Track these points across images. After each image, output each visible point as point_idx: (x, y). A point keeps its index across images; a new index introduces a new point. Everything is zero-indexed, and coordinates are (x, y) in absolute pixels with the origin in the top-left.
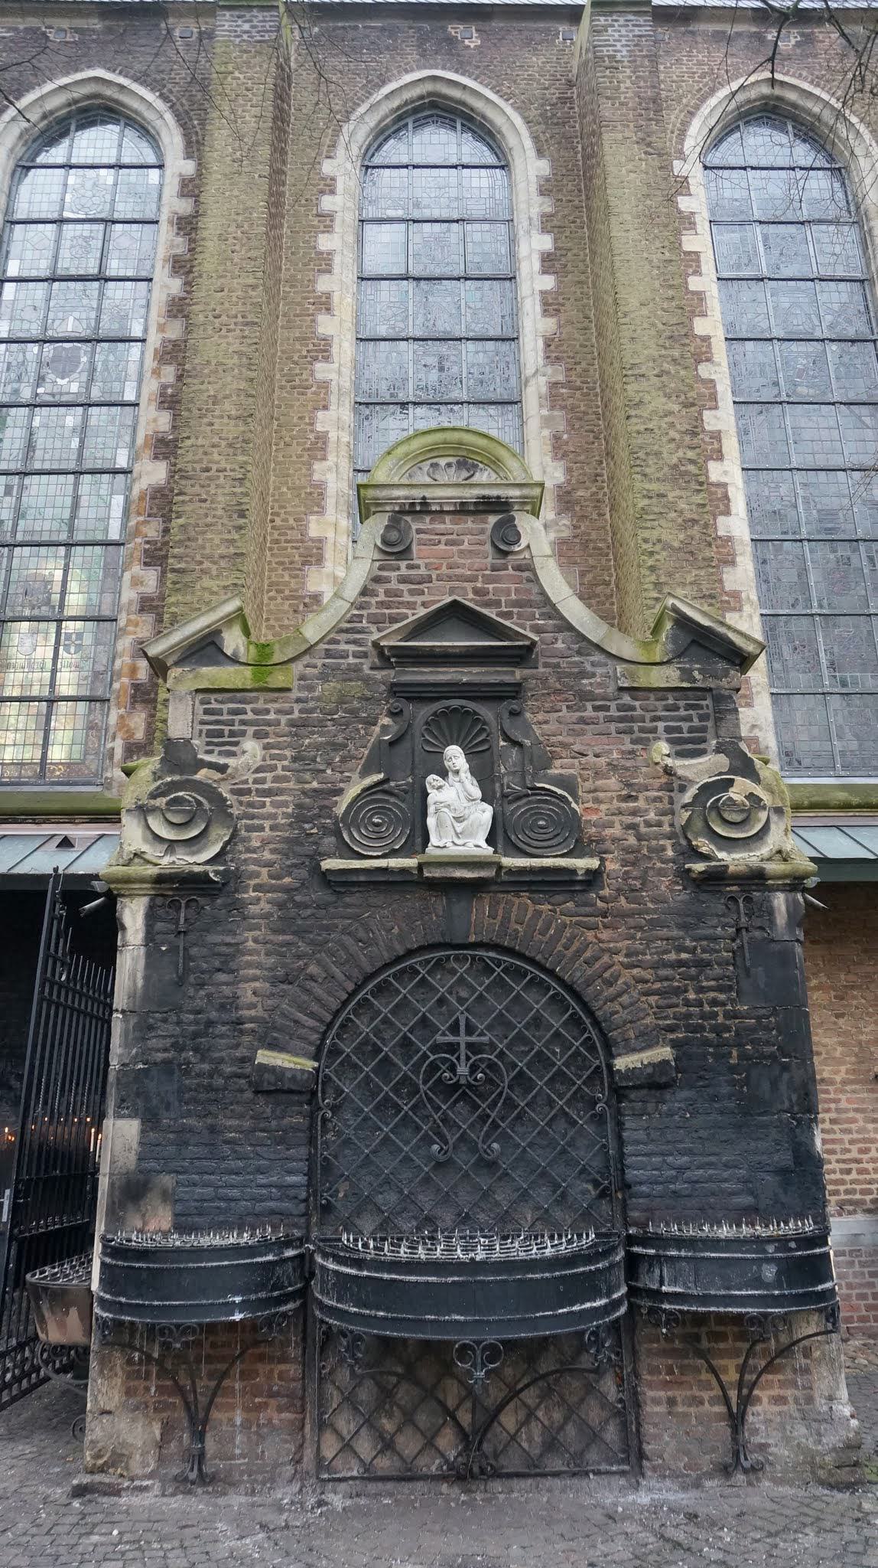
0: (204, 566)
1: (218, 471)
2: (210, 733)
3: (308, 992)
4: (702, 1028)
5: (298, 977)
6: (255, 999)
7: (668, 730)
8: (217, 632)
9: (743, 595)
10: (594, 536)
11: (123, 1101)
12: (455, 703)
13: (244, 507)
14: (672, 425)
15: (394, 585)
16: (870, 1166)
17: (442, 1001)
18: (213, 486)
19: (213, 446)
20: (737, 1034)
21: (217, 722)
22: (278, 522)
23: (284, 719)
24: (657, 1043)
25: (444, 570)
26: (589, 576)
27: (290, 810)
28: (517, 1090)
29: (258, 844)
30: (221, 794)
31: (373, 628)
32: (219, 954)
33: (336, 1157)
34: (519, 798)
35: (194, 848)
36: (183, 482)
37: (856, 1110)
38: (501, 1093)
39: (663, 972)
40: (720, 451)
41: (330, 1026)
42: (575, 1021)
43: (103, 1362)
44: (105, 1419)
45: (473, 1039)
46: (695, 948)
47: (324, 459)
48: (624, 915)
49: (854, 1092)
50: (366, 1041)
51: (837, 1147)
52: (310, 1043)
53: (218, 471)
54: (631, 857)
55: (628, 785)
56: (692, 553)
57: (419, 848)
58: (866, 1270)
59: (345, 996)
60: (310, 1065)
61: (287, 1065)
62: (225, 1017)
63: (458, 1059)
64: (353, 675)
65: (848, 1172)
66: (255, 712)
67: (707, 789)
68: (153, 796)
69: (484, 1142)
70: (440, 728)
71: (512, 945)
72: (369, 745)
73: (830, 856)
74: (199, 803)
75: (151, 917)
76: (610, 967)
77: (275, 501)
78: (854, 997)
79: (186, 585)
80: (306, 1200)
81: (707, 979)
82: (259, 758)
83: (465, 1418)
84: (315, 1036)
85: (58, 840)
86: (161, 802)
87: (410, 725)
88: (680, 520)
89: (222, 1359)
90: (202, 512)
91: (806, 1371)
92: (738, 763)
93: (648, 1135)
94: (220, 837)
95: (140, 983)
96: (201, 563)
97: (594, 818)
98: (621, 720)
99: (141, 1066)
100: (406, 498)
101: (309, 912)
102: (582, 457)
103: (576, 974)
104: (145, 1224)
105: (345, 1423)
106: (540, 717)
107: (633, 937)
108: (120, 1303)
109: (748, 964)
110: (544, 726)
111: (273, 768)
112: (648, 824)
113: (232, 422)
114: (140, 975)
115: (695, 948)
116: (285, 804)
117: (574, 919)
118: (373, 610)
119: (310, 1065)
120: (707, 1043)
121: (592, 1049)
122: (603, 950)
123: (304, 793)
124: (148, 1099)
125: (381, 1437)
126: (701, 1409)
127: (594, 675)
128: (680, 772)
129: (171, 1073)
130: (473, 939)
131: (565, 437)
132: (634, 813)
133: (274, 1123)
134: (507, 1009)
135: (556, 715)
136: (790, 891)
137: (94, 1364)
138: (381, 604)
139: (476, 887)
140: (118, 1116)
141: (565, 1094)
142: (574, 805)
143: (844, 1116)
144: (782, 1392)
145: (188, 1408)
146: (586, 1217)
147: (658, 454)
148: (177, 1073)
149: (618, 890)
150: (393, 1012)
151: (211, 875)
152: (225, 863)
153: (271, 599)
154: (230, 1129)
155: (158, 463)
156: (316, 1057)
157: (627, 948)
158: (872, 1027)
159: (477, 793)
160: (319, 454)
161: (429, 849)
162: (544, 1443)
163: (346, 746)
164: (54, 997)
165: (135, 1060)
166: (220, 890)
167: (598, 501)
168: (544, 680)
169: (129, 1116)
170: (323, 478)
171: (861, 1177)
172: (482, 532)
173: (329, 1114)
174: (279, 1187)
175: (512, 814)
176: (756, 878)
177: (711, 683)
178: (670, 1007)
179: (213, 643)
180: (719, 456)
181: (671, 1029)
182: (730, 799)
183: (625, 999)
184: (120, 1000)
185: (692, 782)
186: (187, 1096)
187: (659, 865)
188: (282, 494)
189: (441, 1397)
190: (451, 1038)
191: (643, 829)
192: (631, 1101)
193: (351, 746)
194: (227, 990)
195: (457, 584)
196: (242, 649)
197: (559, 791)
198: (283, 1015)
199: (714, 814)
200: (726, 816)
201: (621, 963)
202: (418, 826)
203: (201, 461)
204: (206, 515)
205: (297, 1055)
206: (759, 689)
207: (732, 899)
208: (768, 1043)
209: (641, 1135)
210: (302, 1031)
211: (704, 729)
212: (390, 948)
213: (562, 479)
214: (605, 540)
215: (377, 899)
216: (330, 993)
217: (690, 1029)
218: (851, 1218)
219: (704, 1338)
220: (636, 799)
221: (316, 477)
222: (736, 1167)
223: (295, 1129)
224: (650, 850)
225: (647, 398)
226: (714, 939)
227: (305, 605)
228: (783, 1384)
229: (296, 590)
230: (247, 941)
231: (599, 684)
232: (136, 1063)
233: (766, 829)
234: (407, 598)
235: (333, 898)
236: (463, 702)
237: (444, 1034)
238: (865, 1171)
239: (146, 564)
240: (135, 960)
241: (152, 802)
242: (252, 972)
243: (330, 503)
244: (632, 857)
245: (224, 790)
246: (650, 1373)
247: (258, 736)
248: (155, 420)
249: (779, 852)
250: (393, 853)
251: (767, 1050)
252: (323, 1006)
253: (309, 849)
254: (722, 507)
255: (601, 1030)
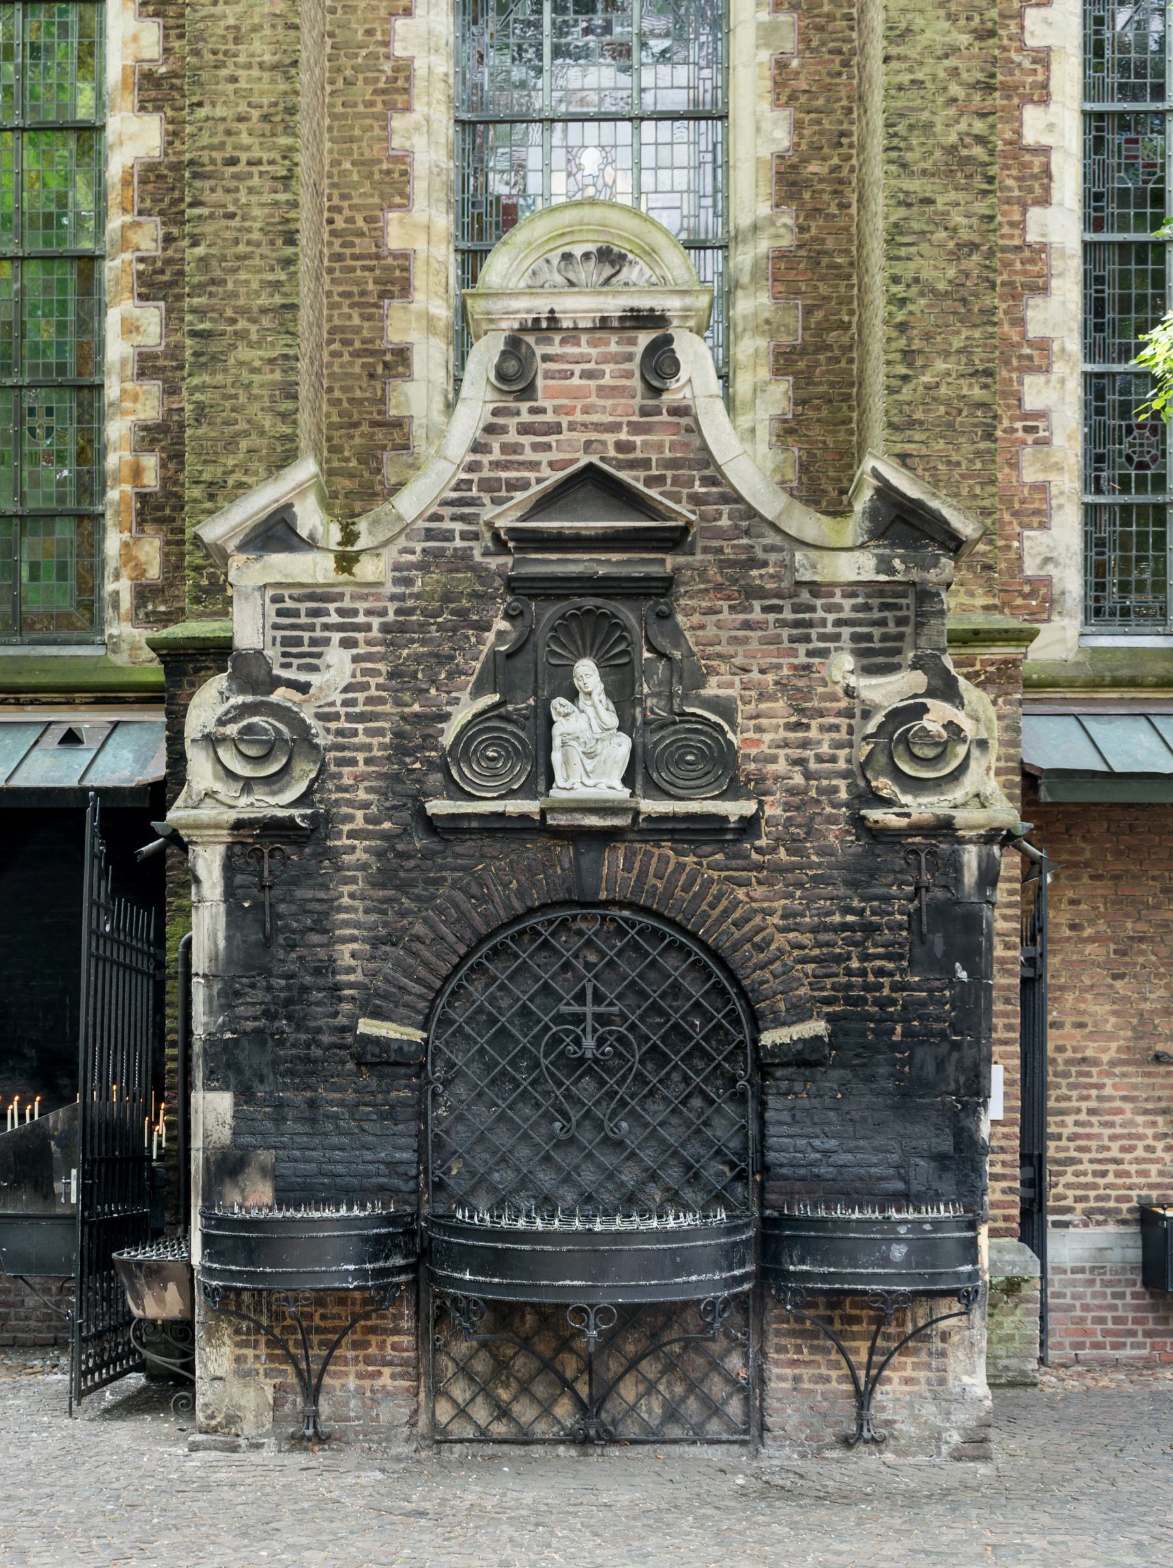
0: (239, 326)
1: (249, 163)
2: (286, 641)
3: (415, 955)
4: (863, 1001)
5: (401, 938)
6: (353, 962)
7: (855, 638)
8: (289, 506)
9: (1056, 346)
10: (830, 244)
11: (212, 1072)
12: (589, 603)
13: (292, 226)
14: (954, 72)
15: (512, 437)
16: (1133, 1168)
17: (567, 966)
18: (243, 192)
19: (240, 119)
20: (904, 1007)
21: (294, 627)
22: (340, 224)
23: (376, 622)
24: (811, 1017)
25: (578, 417)
26: (819, 315)
27: (387, 740)
28: (650, 1066)
29: (351, 782)
30: (303, 721)
31: (486, 499)
32: (310, 912)
33: (447, 1132)
34: (663, 726)
35: (275, 787)
36: (198, 184)
37: (1124, 1098)
38: (631, 1069)
39: (824, 937)
40: (1045, 86)
41: (439, 992)
42: (719, 990)
43: (211, 1333)
44: (216, 1384)
45: (601, 1009)
46: (863, 910)
47: (408, 109)
48: (780, 869)
49: (1124, 1075)
50: (480, 1010)
51: (1093, 1144)
52: (419, 1012)
53: (249, 163)
54: (796, 800)
55: (801, 711)
56: (964, 301)
57: (541, 788)
58: (1109, 1291)
59: (456, 960)
60: (417, 1035)
61: (392, 1035)
62: (321, 981)
63: (584, 1031)
64: (461, 564)
65: (1104, 1174)
66: (341, 612)
67: (898, 716)
68: (221, 722)
69: (610, 1120)
70: (571, 636)
71: (648, 904)
72: (482, 657)
73: (1117, 769)
74: (278, 731)
75: (229, 868)
76: (763, 929)
77: (334, 185)
78: (1142, 953)
79: (214, 358)
80: (416, 1177)
81: (875, 946)
82: (348, 673)
83: (583, 1390)
84: (422, 1005)
85: (58, 732)
86: (232, 730)
87: (532, 631)
88: (951, 245)
89: (334, 1330)
90: (228, 235)
91: (943, 1354)
92: (938, 683)
93: (794, 1116)
94: (306, 773)
95: (222, 944)
96: (233, 321)
97: (753, 751)
98: (797, 624)
99: (229, 1035)
100: (529, 311)
101: (412, 863)
102: (821, 102)
103: (723, 936)
104: (244, 1199)
105: (460, 1391)
106: (696, 619)
107: (791, 896)
108: (230, 1271)
109: (925, 930)
110: (700, 633)
111: (365, 687)
112: (820, 759)
113: (266, 75)
114: (221, 935)
115: (863, 910)
116: (380, 732)
117: (723, 874)
118: (486, 473)
119: (417, 1035)
120: (870, 1017)
121: (736, 1022)
122: (755, 911)
123: (403, 718)
124: (239, 1071)
125: (498, 1406)
126: (828, 1386)
127: (765, 564)
128: (865, 694)
129: (263, 1043)
130: (603, 896)
131: (795, 63)
132: (805, 744)
133: (380, 1096)
134: (640, 976)
135: (715, 618)
136: (986, 843)
137: (199, 1332)
138: (496, 465)
139: (610, 836)
140: (207, 1088)
141: (703, 1070)
142: (730, 736)
143: (1107, 1105)
144: (914, 1374)
145: (299, 1373)
146: (718, 1199)
147: (928, 126)
148: (270, 1043)
149: (777, 840)
150: (511, 978)
151: (298, 820)
152: (312, 805)
153: (333, 354)
154: (331, 1103)
155: (147, 118)
156: (424, 1027)
157: (784, 908)
158: (1162, 992)
159: (613, 720)
160: (400, 99)
161: (553, 792)
162: (664, 1413)
163: (453, 658)
164: (101, 951)
165: (222, 1029)
166: (308, 837)
167: (841, 181)
168: (702, 573)
169: (220, 1089)
170: (407, 145)
171: (1120, 1181)
172: (629, 357)
173: (441, 1088)
174: (387, 1164)
175: (656, 744)
176: (944, 828)
177: (915, 575)
178: (827, 976)
179: (284, 520)
180: (1042, 95)
181: (828, 1001)
182: (923, 729)
183: (777, 966)
184: (200, 963)
185: (878, 707)
186: (282, 1068)
187: (828, 810)
188: (343, 174)
189: (560, 1368)
190: (576, 1008)
191: (813, 766)
192: (776, 1079)
193: (459, 659)
194: (322, 953)
195: (594, 436)
196: (320, 529)
197: (714, 718)
198: (387, 980)
199: (901, 747)
200: (917, 750)
201: (775, 926)
202: (541, 761)
203: (221, 146)
204: (237, 242)
205: (404, 1025)
206: (1062, 500)
207: (914, 852)
208: (938, 1019)
209: (786, 1116)
210: (407, 998)
211: (900, 637)
212: (508, 906)
213: (786, 143)
214: (847, 252)
215: (492, 847)
216: (438, 956)
217: (848, 1001)
218: (1099, 1230)
219: (837, 1321)
220: (807, 727)
221: (396, 142)
222: (888, 1151)
223: (402, 1103)
224: (819, 790)
225: (920, 22)
226: (887, 899)
227: (386, 365)
228: (916, 1367)
229: (371, 341)
230: (341, 895)
231: (772, 576)
232: (223, 1033)
233: (963, 767)
234: (529, 455)
235: (438, 847)
236: (599, 601)
237: (568, 1004)
238: (1127, 1174)
239: (142, 297)
240: (214, 917)
241: (222, 730)
242: (348, 932)
243: (419, 187)
244: (798, 800)
245: (308, 715)
246: (778, 1351)
247: (346, 644)
248: (135, 38)
249: (977, 796)
250: (511, 794)
251: (936, 1026)
252: (432, 971)
253: (414, 787)
254: (1038, 190)
255: (748, 1001)
